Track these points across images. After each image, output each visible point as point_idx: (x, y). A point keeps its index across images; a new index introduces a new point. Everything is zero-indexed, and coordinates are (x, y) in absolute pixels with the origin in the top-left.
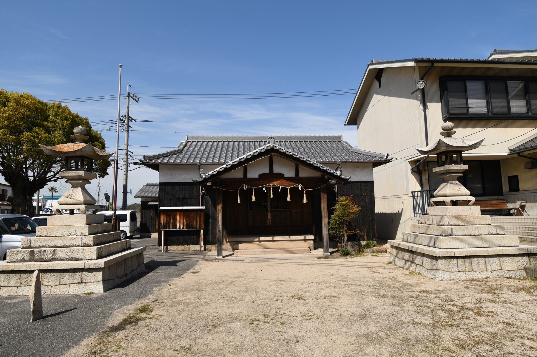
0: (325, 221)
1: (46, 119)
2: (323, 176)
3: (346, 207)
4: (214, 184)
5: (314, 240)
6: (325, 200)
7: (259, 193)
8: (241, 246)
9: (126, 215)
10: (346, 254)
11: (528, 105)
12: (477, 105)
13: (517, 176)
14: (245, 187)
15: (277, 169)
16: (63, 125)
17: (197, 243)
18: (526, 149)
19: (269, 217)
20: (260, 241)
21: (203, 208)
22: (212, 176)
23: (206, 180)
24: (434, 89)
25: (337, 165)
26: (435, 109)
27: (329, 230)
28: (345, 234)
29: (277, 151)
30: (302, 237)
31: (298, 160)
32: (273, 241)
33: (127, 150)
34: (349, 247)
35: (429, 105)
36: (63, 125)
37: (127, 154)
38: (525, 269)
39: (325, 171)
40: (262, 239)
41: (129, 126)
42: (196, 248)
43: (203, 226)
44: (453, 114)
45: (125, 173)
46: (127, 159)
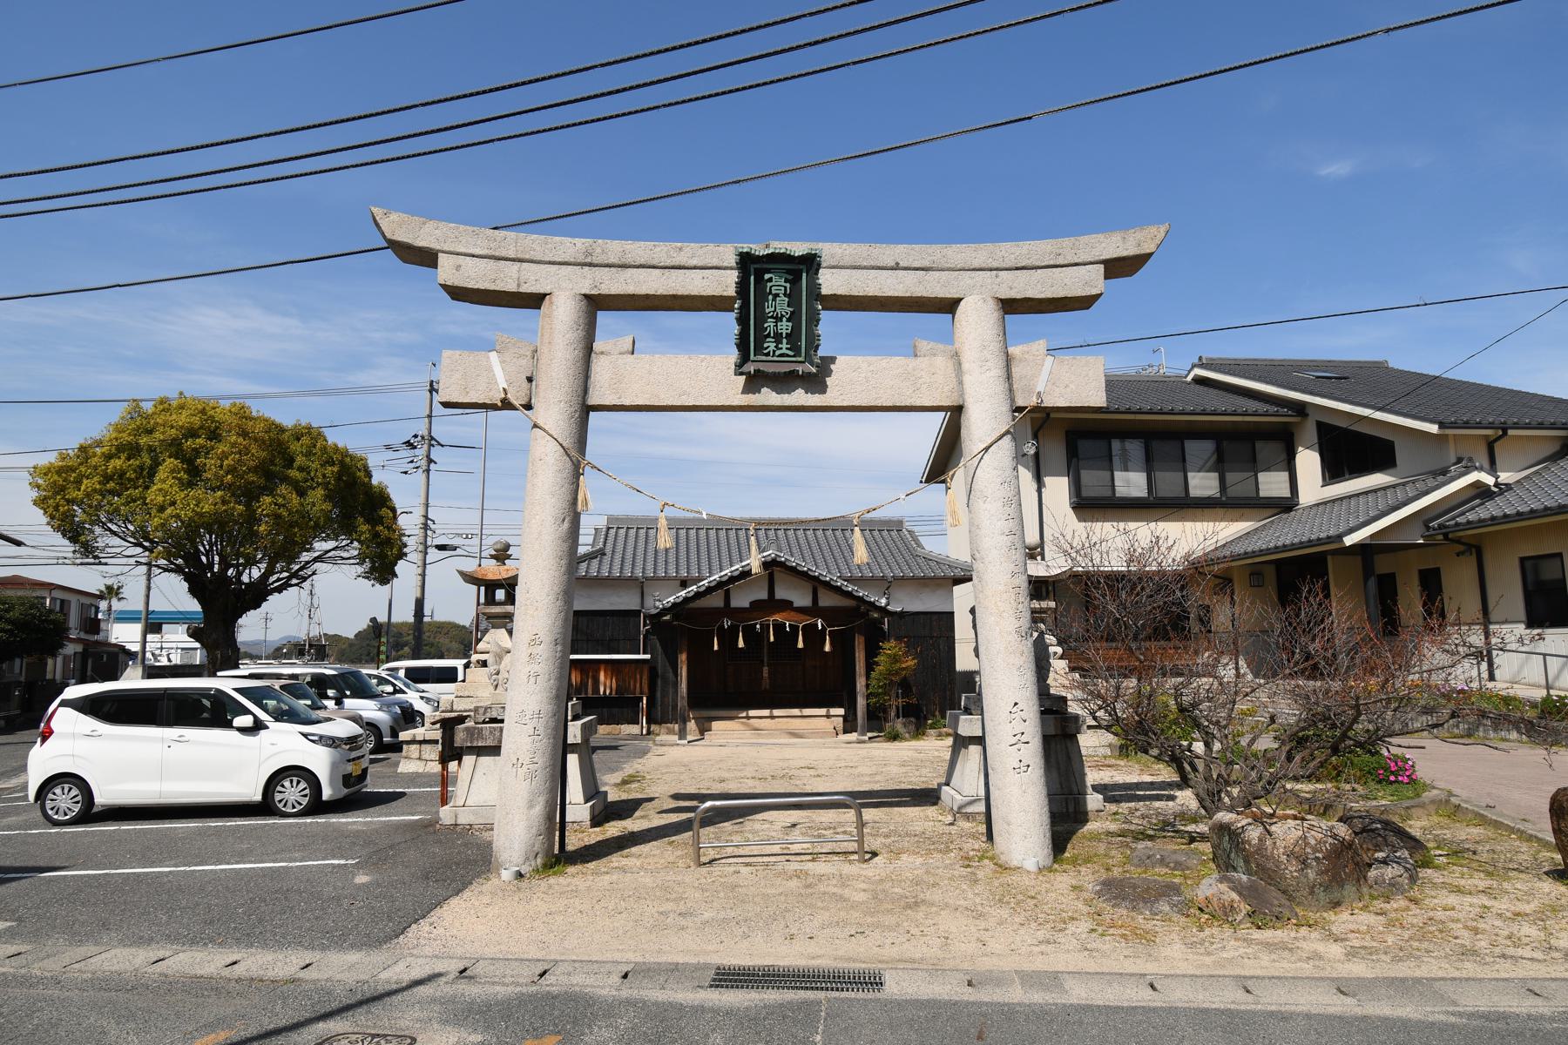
0: (861, 683)
1: (290, 461)
2: (858, 607)
3: (895, 659)
4: (675, 617)
5: (845, 718)
6: (862, 646)
7: (750, 633)
8: (715, 725)
9: (455, 669)
10: (894, 737)
11: (1222, 481)
12: (1131, 483)
13: (1560, 555)
14: (727, 624)
15: (780, 594)
16: (324, 476)
17: (635, 721)
18: (1219, 561)
19: (765, 674)
20: (748, 718)
21: (648, 657)
22: (675, 605)
23: (665, 611)
24: (1056, 451)
25: (887, 584)
26: (1058, 488)
27: (868, 697)
28: (895, 702)
29: (783, 565)
30: (823, 711)
31: (816, 579)
32: (772, 717)
33: (426, 517)
34: (899, 725)
35: (1047, 480)
36: (324, 476)
37: (426, 527)
38: (1110, 745)
39: (861, 599)
40: (752, 713)
41: (430, 461)
42: (634, 729)
43: (646, 689)
44: (1086, 499)
45: (420, 571)
46: (426, 536)
